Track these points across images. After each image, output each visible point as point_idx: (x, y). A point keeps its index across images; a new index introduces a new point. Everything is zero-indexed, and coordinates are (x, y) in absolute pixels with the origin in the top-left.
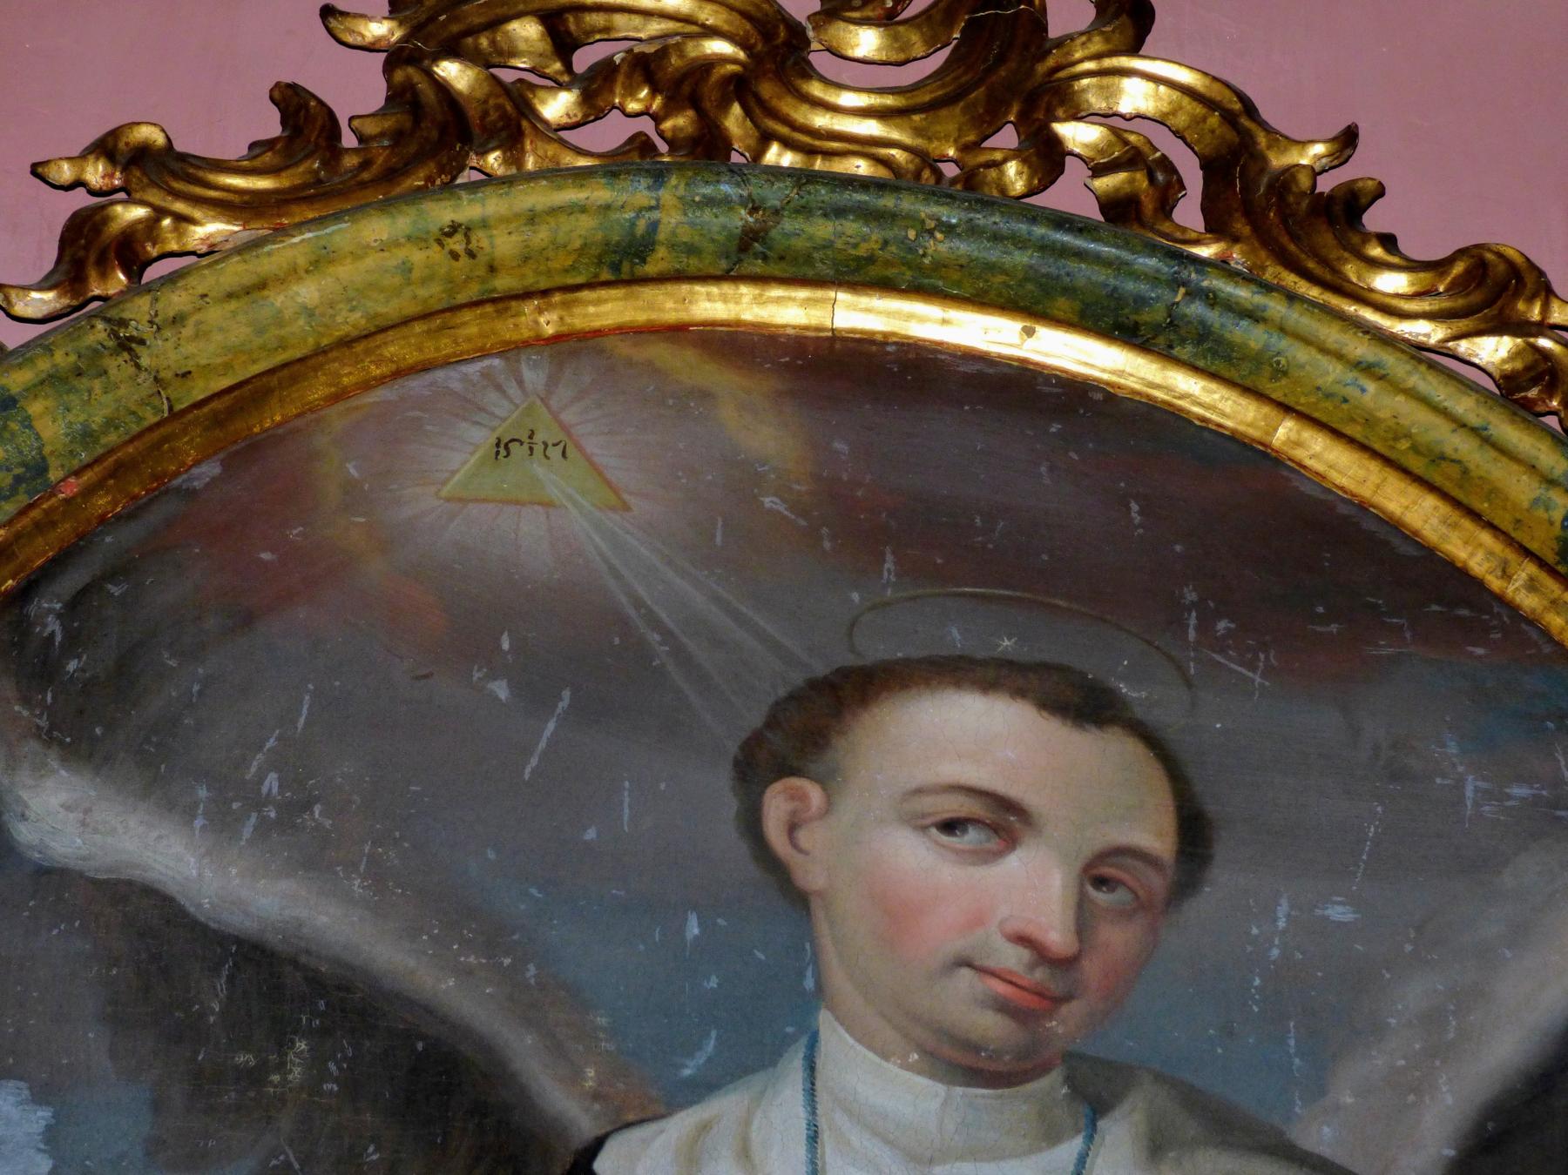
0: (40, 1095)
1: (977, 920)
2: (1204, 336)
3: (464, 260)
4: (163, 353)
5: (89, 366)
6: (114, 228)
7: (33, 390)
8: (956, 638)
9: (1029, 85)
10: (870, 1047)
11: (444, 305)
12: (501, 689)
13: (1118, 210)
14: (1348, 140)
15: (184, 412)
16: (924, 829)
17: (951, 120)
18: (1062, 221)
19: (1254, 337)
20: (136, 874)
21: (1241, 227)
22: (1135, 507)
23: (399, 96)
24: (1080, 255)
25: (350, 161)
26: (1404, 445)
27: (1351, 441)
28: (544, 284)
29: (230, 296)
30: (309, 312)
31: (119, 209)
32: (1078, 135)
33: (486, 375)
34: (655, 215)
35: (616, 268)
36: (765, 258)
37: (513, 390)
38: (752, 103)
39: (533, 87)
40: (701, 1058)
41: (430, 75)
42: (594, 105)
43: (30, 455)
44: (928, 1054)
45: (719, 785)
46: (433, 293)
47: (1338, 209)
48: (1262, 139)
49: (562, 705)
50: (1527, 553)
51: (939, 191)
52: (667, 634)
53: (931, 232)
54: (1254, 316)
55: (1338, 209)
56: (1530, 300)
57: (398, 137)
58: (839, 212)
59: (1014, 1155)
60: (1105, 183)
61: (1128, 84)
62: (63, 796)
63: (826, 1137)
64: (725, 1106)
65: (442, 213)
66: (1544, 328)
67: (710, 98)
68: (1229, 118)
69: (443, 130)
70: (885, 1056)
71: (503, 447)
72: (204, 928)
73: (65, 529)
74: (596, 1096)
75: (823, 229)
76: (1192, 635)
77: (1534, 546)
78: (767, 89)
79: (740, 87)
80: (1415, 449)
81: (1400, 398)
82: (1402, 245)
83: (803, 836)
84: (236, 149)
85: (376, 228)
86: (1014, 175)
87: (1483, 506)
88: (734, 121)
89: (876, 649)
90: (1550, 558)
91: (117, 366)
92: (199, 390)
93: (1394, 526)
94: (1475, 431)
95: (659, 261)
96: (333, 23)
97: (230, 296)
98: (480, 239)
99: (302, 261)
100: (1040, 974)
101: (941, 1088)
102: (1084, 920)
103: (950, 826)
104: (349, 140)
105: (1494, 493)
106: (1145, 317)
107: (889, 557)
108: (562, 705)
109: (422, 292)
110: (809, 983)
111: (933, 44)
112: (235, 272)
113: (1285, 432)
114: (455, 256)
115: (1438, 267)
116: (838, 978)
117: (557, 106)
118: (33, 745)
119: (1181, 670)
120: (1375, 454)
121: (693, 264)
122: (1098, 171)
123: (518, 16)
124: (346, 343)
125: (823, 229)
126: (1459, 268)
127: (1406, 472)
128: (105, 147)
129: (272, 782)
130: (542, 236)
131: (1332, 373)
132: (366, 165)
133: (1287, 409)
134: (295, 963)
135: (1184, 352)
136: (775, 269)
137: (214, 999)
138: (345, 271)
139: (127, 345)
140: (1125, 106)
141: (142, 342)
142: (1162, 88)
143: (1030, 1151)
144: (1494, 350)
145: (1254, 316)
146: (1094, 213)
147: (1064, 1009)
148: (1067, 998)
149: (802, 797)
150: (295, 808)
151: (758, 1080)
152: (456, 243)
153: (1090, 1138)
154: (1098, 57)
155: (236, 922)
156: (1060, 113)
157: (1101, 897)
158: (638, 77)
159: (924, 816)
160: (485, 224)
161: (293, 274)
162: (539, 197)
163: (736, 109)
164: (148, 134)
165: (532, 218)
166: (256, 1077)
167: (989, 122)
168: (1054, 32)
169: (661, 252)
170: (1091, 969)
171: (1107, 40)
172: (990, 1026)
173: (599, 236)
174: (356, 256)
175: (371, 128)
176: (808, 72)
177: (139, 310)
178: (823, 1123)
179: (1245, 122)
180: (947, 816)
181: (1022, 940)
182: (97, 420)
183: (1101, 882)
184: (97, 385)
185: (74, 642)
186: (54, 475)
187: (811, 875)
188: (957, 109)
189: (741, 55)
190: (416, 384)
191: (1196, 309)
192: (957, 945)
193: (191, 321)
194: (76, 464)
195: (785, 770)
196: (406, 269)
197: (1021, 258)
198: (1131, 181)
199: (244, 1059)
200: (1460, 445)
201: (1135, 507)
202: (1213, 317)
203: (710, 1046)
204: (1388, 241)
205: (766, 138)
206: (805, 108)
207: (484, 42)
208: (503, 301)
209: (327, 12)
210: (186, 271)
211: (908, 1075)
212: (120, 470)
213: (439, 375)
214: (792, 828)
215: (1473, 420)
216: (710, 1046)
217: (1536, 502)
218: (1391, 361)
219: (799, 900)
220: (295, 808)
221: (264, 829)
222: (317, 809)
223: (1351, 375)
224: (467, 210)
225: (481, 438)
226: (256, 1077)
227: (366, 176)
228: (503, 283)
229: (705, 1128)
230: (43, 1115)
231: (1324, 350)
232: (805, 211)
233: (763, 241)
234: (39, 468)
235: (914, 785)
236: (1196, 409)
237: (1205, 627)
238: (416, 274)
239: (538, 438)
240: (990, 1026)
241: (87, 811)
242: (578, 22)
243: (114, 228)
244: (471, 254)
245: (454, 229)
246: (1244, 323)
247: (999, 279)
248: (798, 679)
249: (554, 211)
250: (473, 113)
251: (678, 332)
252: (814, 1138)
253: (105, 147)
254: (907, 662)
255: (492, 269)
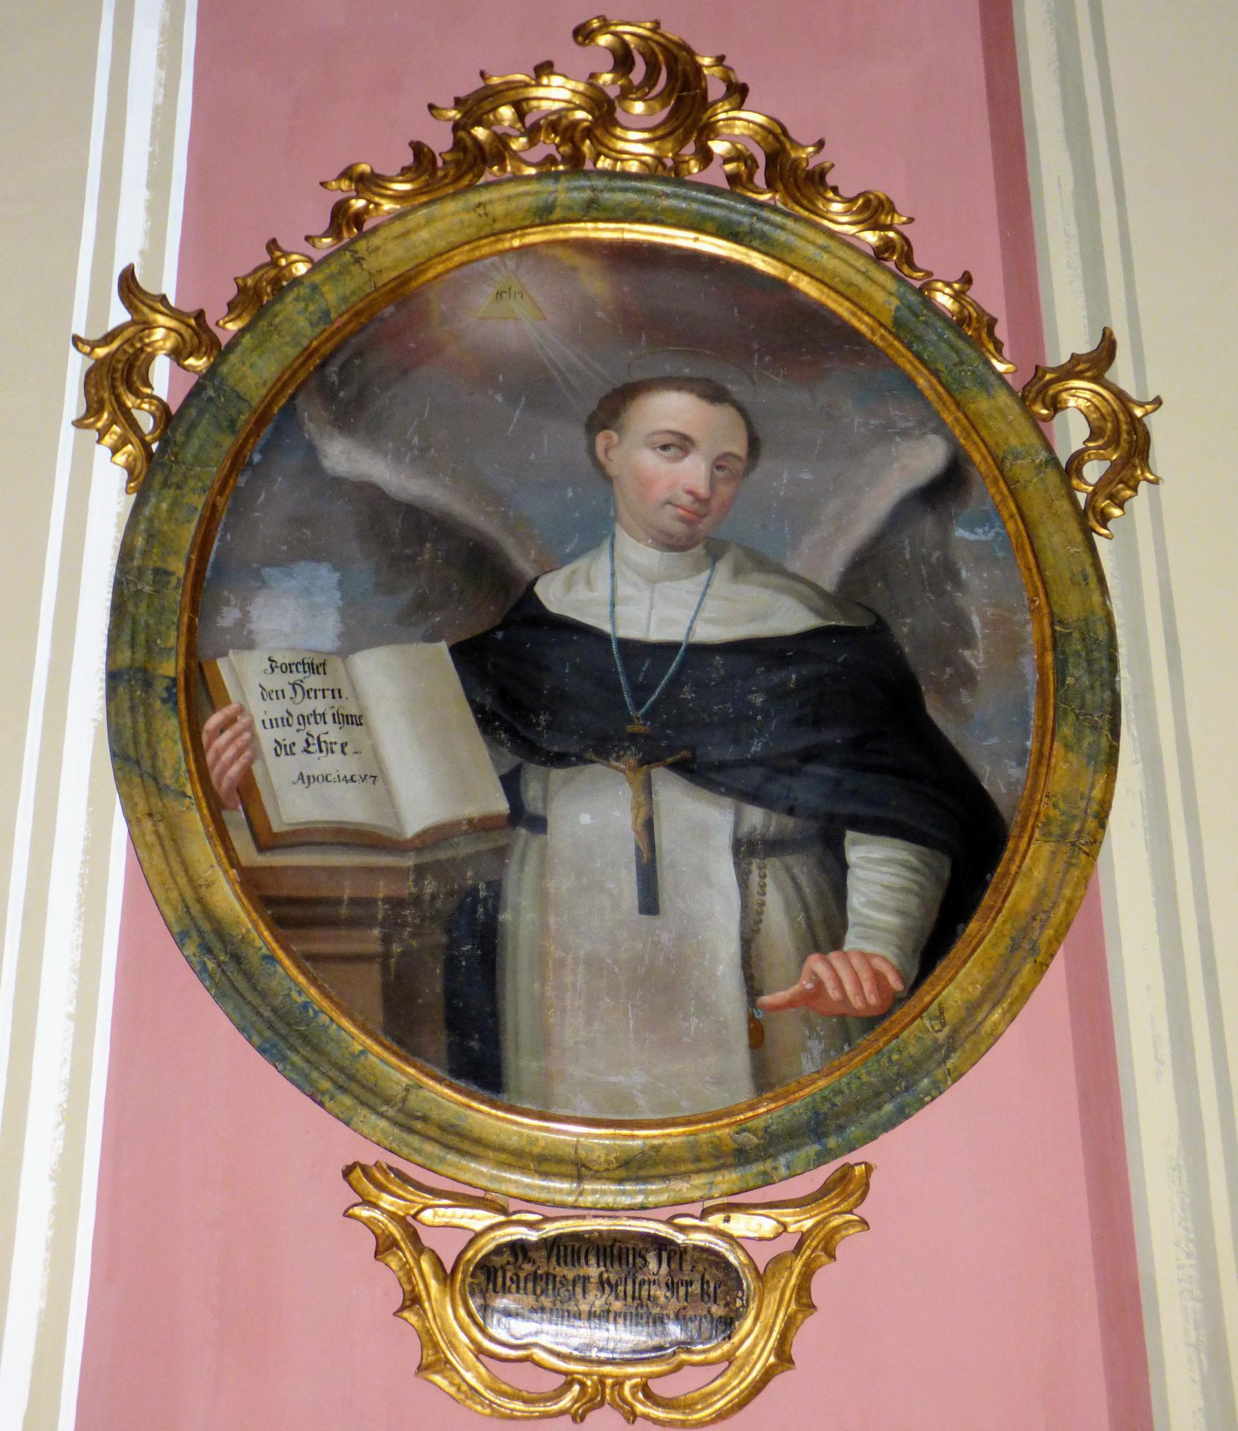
0: (336, 568)
1: (672, 486)
2: (763, 236)
3: (483, 217)
4: (372, 263)
5: (344, 270)
6: (353, 210)
7: (324, 282)
8: (668, 369)
9: (701, 124)
10: (634, 538)
11: (476, 236)
12: (499, 398)
13: (733, 179)
14: (820, 145)
15: (381, 288)
16: (654, 449)
17: (669, 145)
18: (711, 190)
19: (781, 236)
20: (364, 479)
21: (780, 186)
22: (736, 310)
23: (458, 145)
24: (715, 204)
25: (440, 174)
26: (837, 279)
27: (818, 280)
28: (514, 226)
29: (397, 237)
30: (425, 242)
31: (353, 201)
32: (719, 147)
33: (493, 264)
34: (556, 194)
35: (541, 218)
36: (597, 210)
37: (503, 269)
38: (595, 141)
39: (510, 136)
40: (573, 545)
41: (470, 134)
42: (532, 142)
43: (324, 307)
44: (654, 539)
45: (578, 434)
46: (471, 232)
47: (816, 177)
48: (788, 145)
49: (522, 403)
50: (881, 325)
51: (665, 180)
52: (559, 370)
53: (660, 197)
54: (782, 227)
55: (816, 177)
56: (887, 214)
57: (458, 163)
58: (625, 190)
59: (686, 578)
60: (729, 167)
61: (738, 123)
62: (340, 448)
63: (618, 574)
64: (581, 563)
65: (474, 198)
66: (890, 227)
67: (578, 135)
68: (776, 137)
69: (475, 159)
70: (639, 541)
71: (499, 295)
72: (394, 501)
73: (338, 338)
74: (535, 561)
75: (619, 197)
76: (756, 363)
77: (883, 321)
78: (598, 133)
79: (588, 133)
80: (842, 281)
81: (836, 261)
82: (841, 191)
83: (611, 454)
84: (394, 170)
85: (450, 206)
86: (694, 167)
87: (865, 304)
88: (587, 146)
89: (638, 375)
90: (890, 326)
91: (355, 269)
92: (386, 277)
93: (833, 313)
94: (864, 273)
95: (557, 214)
96: (434, 112)
97: (397, 237)
98: (490, 208)
99: (422, 222)
100: (696, 506)
101: (658, 553)
102: (713, 483)
103: (665, 447)
104: (440, 163)
105: (870, 299)
106: (741, 229)
107: (644, 336)
108: (522, 403)
109: (468, 231)
110: (612, 514)
111: (663, 106)
112: (398, 227)
113: (793, 277)
114: (480, 215)
115: (851, 201)
116: (622, 510)
117: (518, 144)
118: (328, 427)
119: (750, 376)
120: (826, 285)
121: (570, 215)
122: (727, 160)
123: (504, 104)
124: (440, 254)
125: (619, 197)
126: (860, 202)
127: (837, 292)
128: (347, 174)
129: (416, 440)
130: (513, 204)
131: (811, 250)
132: (446, 176)
133: (794, 267)
134: (426, 513)
135: (755, 243)
136: (602, 215)
137: (396, 526)
138: (439, 225)
139: (358, 260)
140: (737, 131)
141: (363, 259)
142: (751, 125)
143: (691, 576)
144: (872, 237)
145: (782, 227)
146: (725, 185)
147: (705, 520)
148: (705, 515)
149: (610, 438)
150: (424, 450)
151: (593, 552)
152: (481, 211)
153: (713, 570)
154: (727, 111)
155: (404, 496)
156: (712, 136)
157: (719, 474)
158: (550, 130)
159: (654, 443)
160: (491, 202)
161: (419, 227)
162: (510, 190)
163: (588, 142)
164: (365, 168)
165: (509, 198)
166: (412, 558)
167: (682, 143)
168: (710, 99)
169: (558, 209)
170: (715, 504)
171: (730, 104)
172: (678, 528)
173: (535, 205)
174: (443, 218)
175: (448, 157)
176: (616, 123)
177: (362, 246)
178: (616, 569)
179: (782, 138)
180: (663, 443)
181: (690, 492)
182: (348, 293)
183: (719, 467)
184: (348, 278)
185: (343, 384)
186: (333, 315)
187: (613, 470)
188: (671, 139)
189: (590, 117)
190: (466, 269)
191: (759, 225)
192: (665, 495)
193: (382, 248)
194: (340, 311)
195: (604, 427)
196: (462, 222)
197: (695, 206)
198: (738, 167)
199: (408, 551)
200: (858, 279)
201: (736, 310)
202: (766, 228)
203: (576, 540)
204: (835, 190)
205: (598, 155)
206: (614, 140)
207: (491, 117)
208: (498, 234)
209: (431, 107)
210: (413, 273)
211: (647, 548)
212: (358, 314)
213: (475, 265)
214: (606, 451)
215: (863, 269)
216: (576, 540)
217: (885, 302)
218: (833, 244)
219: (608, 479)
220: (424, 450)
221: (413, 459)
222: (432, 450)
223: (817, 251)
224: (485, 196)
225: (490, 291)
226: (412, 558)
227: (446, 181)
228: (498, 226)
229: (574, 572)
230: (338, 575)
231: (808, 241)
232: (612, 190)
233: (597, 203)
234: (327, 313)
235: (651, 431)
236: (320, 825)
237: (761, 359)
238: (466, 224)
239: (513, 289)
240: (678, 528)
241: (349, 454)
242: (527, 105)
243: (353, 210)
244: (486, 215)
245: (479, 205)
246: (778, 231)
247: (686, 215)
248: (609, 389)
249: (518, 195)
250: (487, 148)
251: (564, 243)
252: (613, 575)
253: (347, 174)
254: (650, 380)
255: (494, 220)
